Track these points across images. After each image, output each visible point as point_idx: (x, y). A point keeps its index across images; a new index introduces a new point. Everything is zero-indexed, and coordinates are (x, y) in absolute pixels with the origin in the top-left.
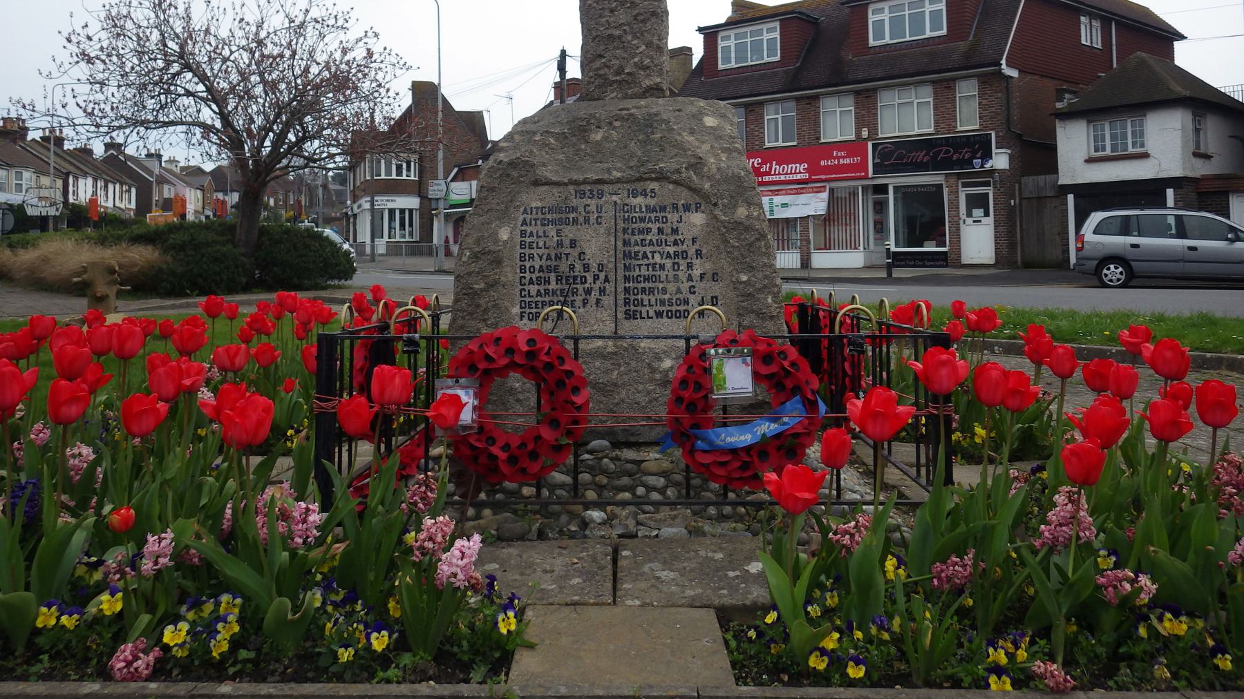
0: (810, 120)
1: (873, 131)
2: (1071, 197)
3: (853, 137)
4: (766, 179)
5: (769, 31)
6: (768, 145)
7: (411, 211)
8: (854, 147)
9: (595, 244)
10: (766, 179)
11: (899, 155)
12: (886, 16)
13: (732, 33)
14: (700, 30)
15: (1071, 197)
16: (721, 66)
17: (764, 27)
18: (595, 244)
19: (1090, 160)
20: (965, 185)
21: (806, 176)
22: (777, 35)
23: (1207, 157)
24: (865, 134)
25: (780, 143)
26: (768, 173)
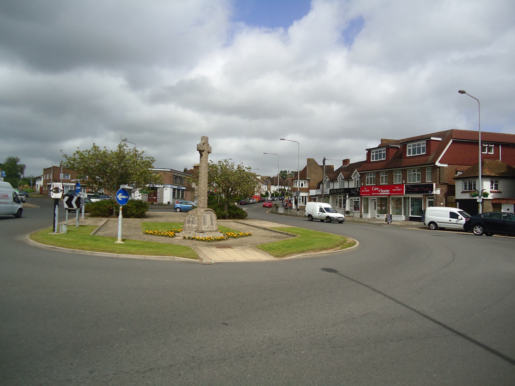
0: (390, 178)
1: (406, 182)
2: (458, 203)
3: (401, 183)
4: (380, 194)
5: (423, 144)
6: (381, 184)
7: (305, 197)
8: (401, 186)
9: (191, 219)
10: (380, 194)
11: (411, 189)
12: (411, 148)
13: (411, 144)
14: (367, 150)
15: (458, 203)
16: (371, 161)
17: (421, 143)
18: (191, 219)
19: (463, 192)
20: (429, 198)
21: (389, 194)
22: (425, 145)
23: (500, 192)
24: (404, 182)
25: (384, 184)
26: (380, 192)
